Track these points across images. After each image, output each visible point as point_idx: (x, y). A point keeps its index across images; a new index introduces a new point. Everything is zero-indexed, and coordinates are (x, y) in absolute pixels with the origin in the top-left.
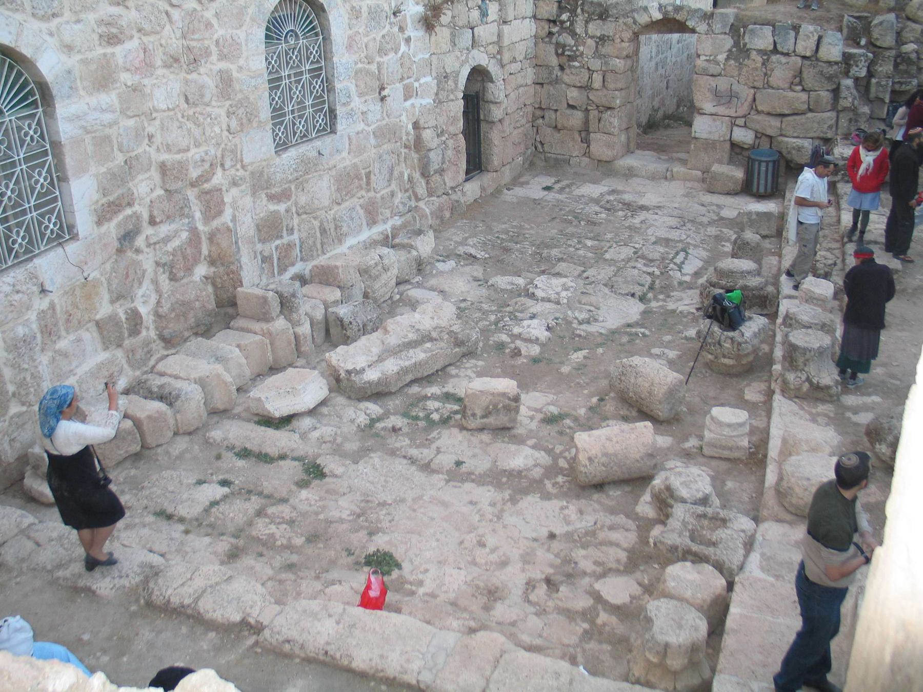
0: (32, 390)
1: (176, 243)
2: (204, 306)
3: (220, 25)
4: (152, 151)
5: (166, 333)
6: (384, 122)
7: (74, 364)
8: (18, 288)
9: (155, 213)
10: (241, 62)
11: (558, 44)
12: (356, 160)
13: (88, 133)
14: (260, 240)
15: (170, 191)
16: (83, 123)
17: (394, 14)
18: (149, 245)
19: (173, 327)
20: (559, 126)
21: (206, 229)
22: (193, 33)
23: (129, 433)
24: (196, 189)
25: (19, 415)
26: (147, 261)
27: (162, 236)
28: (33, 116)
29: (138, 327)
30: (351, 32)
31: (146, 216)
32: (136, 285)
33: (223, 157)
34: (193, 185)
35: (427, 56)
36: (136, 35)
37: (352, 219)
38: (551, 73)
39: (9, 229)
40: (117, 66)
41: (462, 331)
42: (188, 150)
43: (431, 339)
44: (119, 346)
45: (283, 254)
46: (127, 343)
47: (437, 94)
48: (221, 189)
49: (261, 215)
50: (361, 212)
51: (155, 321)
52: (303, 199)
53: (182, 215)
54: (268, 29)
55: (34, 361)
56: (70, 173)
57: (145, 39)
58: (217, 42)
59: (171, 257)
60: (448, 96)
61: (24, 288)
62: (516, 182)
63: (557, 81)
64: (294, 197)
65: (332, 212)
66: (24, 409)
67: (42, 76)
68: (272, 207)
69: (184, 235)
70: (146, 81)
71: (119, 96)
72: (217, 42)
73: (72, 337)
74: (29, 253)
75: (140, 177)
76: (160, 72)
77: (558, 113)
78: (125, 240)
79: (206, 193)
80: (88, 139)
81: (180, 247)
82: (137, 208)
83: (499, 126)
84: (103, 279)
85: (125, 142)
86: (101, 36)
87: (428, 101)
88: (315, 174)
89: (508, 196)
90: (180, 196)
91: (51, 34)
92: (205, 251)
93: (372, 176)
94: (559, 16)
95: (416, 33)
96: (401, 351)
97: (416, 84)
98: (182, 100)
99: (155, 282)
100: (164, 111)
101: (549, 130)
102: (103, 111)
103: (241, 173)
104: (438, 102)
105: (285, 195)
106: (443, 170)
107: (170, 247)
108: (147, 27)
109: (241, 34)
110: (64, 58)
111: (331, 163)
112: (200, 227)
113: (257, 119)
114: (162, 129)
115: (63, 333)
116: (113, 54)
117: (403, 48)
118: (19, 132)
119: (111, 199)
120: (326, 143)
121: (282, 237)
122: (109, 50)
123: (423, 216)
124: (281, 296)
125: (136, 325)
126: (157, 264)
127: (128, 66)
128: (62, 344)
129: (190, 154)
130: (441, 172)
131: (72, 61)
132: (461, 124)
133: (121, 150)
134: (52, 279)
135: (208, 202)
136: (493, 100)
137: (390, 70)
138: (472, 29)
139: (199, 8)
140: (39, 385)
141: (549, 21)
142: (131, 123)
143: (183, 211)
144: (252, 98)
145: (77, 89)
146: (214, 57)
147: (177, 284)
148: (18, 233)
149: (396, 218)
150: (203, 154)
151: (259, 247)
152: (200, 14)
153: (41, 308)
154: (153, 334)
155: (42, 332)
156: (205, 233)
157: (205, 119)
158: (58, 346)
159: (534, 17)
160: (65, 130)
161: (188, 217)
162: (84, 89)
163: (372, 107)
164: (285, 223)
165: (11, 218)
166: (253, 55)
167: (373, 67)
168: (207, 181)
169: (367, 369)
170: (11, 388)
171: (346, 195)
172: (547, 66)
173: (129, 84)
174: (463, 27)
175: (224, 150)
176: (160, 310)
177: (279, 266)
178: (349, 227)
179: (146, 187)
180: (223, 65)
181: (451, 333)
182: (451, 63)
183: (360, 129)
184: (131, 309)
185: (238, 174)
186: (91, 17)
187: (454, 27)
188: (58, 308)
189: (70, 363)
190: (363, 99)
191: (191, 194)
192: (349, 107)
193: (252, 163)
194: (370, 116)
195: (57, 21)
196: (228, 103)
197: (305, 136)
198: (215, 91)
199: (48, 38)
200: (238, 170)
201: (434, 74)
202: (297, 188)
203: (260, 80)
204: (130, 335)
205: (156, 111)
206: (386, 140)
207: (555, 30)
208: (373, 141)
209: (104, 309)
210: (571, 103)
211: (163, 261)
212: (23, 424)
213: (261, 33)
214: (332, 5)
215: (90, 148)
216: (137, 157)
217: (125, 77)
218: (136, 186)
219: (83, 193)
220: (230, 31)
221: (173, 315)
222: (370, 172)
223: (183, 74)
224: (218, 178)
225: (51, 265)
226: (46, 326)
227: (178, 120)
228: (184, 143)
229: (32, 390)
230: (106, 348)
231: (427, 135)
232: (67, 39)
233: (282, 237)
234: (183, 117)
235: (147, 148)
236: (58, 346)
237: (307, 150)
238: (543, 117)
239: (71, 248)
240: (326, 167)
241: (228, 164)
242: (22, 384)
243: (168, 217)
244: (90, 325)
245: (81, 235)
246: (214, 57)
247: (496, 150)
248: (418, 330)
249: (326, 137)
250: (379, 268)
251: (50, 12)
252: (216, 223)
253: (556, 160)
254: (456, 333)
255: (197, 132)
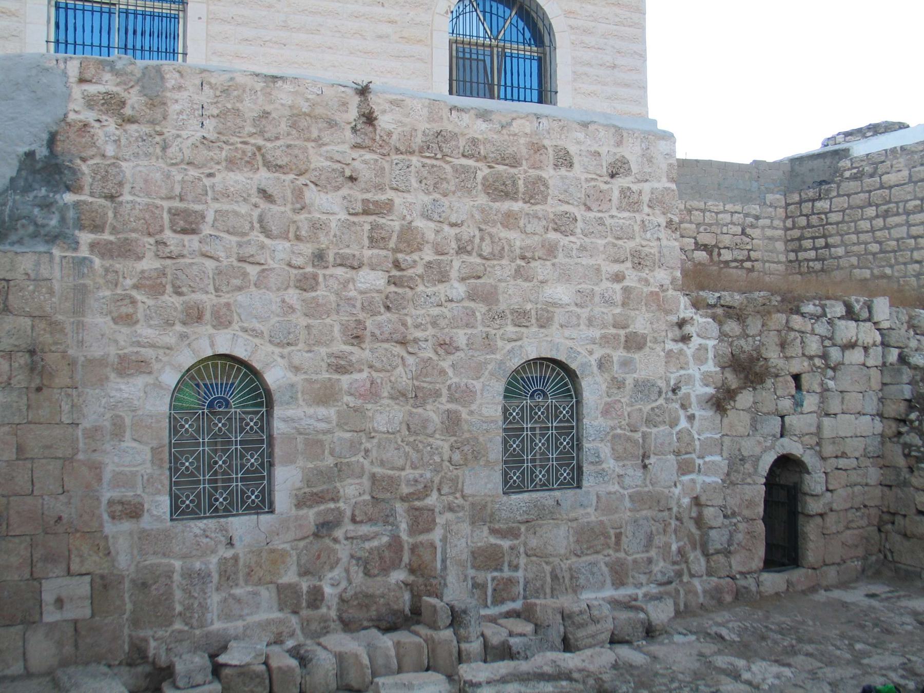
0: (196, 615)
1: (375, 543)
2: (388, 604)
3: (455, 374)
4: (366, 463)
5: (345, 616)
6: (646, 489)
7: (246, 611)
8: (208, 533)
9: (357, 513)
10: (474, 407)
11: (906, 445)
12: (604, 518)
13: (301, 434)
14: (473, 567)
15: (377, 499)
16: (296, 425)
17: (674, 391)
18: (347, 539)
19: (353, 613)
20: (908, 533)
21: (411, 540)
22: (426, 375)
23: (258, 675)
24: (406, 505)
25: (180, 632)
26: (343, 551)
27: (360, 533)
28: (257, 413)
29: (318, 603)
30: (609, 400)
31: (348, 513)
32: (327, 567)
33: (440, 483)
34: (403, 499)
35: (718, 436)
36: (366, 370)
37: (593, 574)
38: (898, 475)
39: (216, 489)
40: (341, 390)
41: (612, 681)
42: (403, 469)
43: (570, 678)
44: (295, 612)
45: (501, 586)
46: (305, 613)
47: (728, 474)
48: (433, 510)
49: (479, 544)
50: (605, 569)
51: (338, 604)
52: (533, 542)
53: (386, 523)
54: (509, 383)
55: (205, 593)
56: (277, 461)
57: (375, 374)
58: (449, 387)
59: (367, 554)
60: (743, 480)
61: (213, 535)
62: (844, 585)
63: (905, 484)
64: (523, 538)
65: (569, 562)
66: (186, 628)
67: (267, 385)
68: (493, 540)
69: (385, 539)
70: (369, 406)
71: (338, 412)
72: (449, 387)
73: (249, 589)
74: (228, 512)
75: (349, 481)
76: (386, 401)
77: (907, 519)
78: (323, 527)
79: (416, 509)
80: (300, 439)
81: (378, 548)
82: (341, 505)
83: (819, 520)
84: (294, 553)
85: (337, 449)
86: (329, 365)
87: (715, 479)
88: (551, 521)
89: (822, 596)
90: (387, 506)
91: (282, 357)
92: (406, 558)
93: (623, 538)
94: (907, 415)
95: (704, 414)
96: (529, 680)
97: (701, 461)
98: (404, 427)
99: (347, 571)
100: (384, 433)
101: (898, 538)
102: (318, 420)
103: (460, 501)
104: (729, 482)
105: (512, 533)
106: (730, 552)
107: (367, 545)
108: (378, 365)
109: (478, 385)
110: (290, 375)
111: (572, 515)
112: (404, 536)
113: (485, 458)
114: (379, 447)
115: (241, 582)
116: (339, 380)
117: (683, 424)
118: (241, 422)
119: (315, 490)
120: (567, 496)
121: (501, 570)
122: (336, 376)
123: (690, 591)
124: (452, 608)
125: (315, 600)
126: (352, 556)
127: (352, 391)
128: (237, 591)
129: (403, 473)
130: (727, 553)
131: (298, 379)
132: (761, 509)
133: (332, 453)
134: (241, 537)
135: (416, 517)
136: (809, 492)
137: (659, 441)
138: (782, 417)
139: (435, 358)
140: (203, 614)
141: (896, 419)
142: (348, 435)
143: (388, 519)
144: (481, 439)
145: (297, 399)
146: (444, 399)
147: (369, 580)
148: (221, 494)
149: (652, 585)
150: (417, 476)
151: (471, 572)
152: (436, 362)
153: (225, 555)
154: (333, 614)
155: (220, 575)
156: (408, 543)
157: (424, 447)
158: (233, 591)
159: (881, 415)
160: (279, 427)
161: (392, 524)
162: (304, 400)
163: (630, 472)
164: (506, 559)
165: (220, 481)
166: (488, 403)
167: (638, 436)
168: (418, 499)
169: (484, 684)
170: (178, 608)
171: (588, 549)
172: (895, 467)
173: (351, 405)
174: (769, 414)
175: (442, 478)
176: (344, 595)
177: (494, 597)
178: (588, 580)
179: (352, 491)
180: (450, 406)
181: (598, 680)
182: (749, 447)
183: (613, 490)
184: (315, 587)
185: (456, 501)
186: (323, 351)
187: (756, 415)
188: (241, 562)
189: (242, 609)
190: (621, 464)
191: (400, 507)
192: (600, 467)
193: (474, 496)
194: (627, 481)
195: (290, 348)
196: (453, 439)
197: (544, 485)
198: (439, 426)
199: (279, 359)
200: (456, 498)
201: (725, 454)
202: (527, 530)
203: (493, 426)
204: (308, 607)
205: (376, 431)
206: (647, 506)
207: (904, 429)
208: (627, 503)
209: (290, 577)
210: (920, 508)
211: (359, 554)
212: (181, 641)
213: (499, 387)
214: (587, 372)
215: (301, 447)
216: (348, 464)
217: (347, 399)
218: (343, 487)
219: (286, 479)
220: (465, 380)
221: (355, 603)
222: (621, 533)
223: (408, 407)
224: (432, 500)
225: (241, 526)
226: (226, 571)
227: (396, 442)
228: (401, 462)
229: (196, 615)
230: (281, 610)
231: (709, 512)
232: (296, 361)
233: (501, 570)
234: (402, 441)
235: (362, 460)
236: (233, 591)
237: (545, 498)
238: (893, 523)
239: (264, 518)
240: (565, 517)
241: (445, 490)
242: (189, 608)
243: (370, 520)
244: (270, 586)
245: (277, 510)
246: (444, 399)
247: (811, 545)
248: (559, 666)
249: (569, 491)
250: (585, 617)
251: (285, 341)
252: (423, 538)
253: (906, 571)
254: (604, 682)
255: (414, 455)
